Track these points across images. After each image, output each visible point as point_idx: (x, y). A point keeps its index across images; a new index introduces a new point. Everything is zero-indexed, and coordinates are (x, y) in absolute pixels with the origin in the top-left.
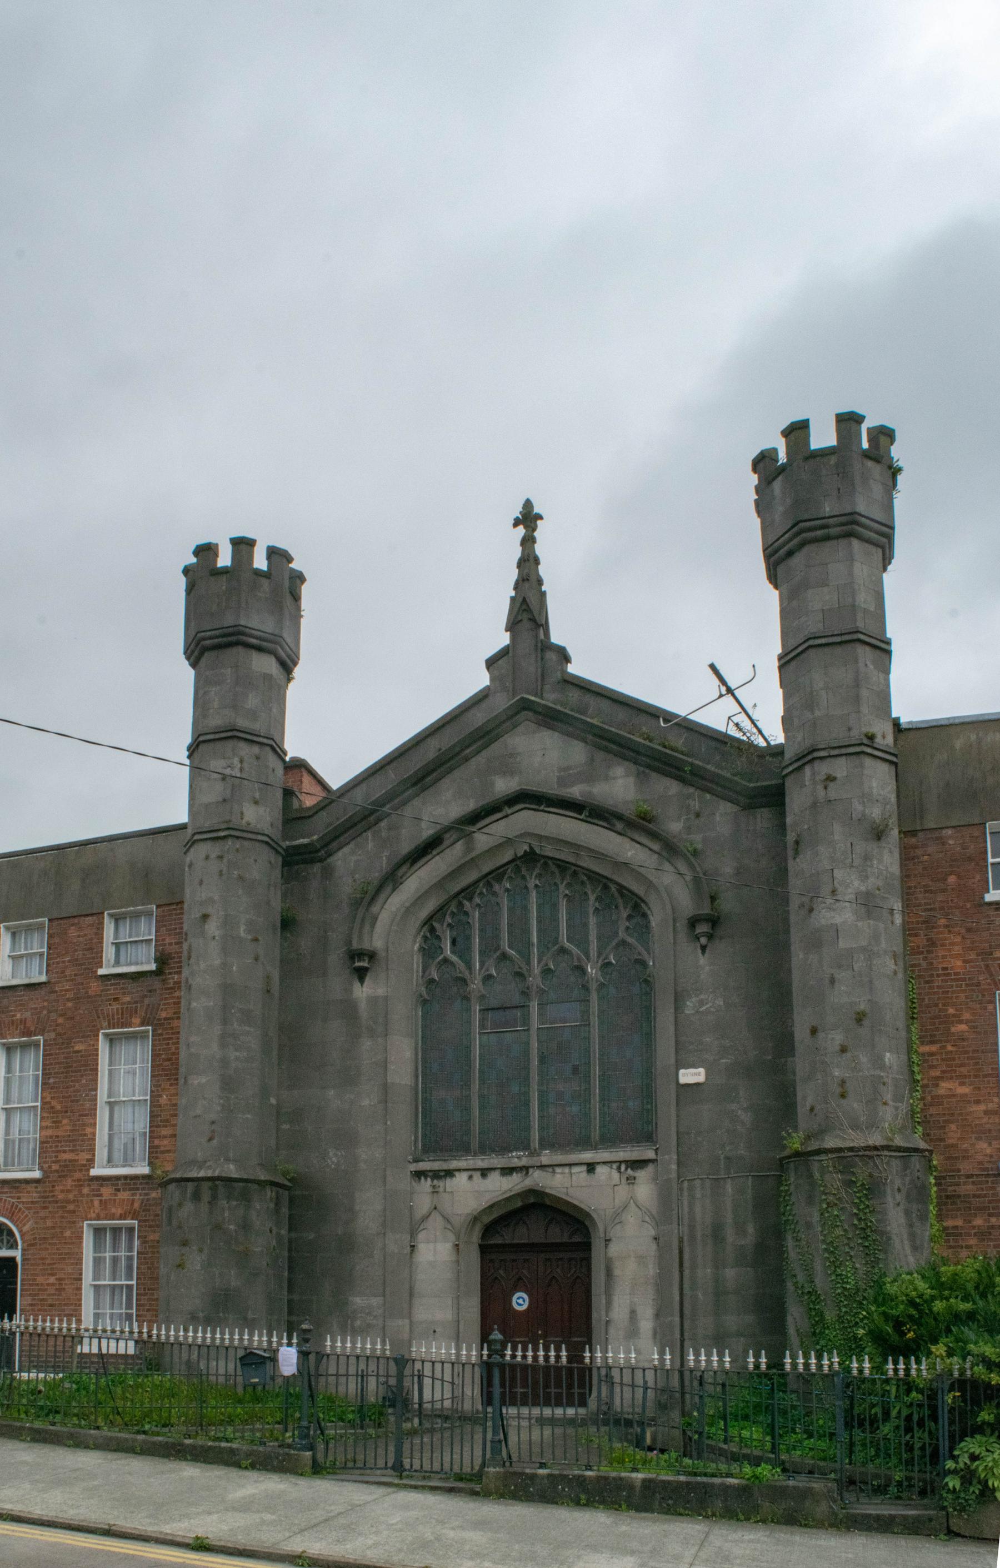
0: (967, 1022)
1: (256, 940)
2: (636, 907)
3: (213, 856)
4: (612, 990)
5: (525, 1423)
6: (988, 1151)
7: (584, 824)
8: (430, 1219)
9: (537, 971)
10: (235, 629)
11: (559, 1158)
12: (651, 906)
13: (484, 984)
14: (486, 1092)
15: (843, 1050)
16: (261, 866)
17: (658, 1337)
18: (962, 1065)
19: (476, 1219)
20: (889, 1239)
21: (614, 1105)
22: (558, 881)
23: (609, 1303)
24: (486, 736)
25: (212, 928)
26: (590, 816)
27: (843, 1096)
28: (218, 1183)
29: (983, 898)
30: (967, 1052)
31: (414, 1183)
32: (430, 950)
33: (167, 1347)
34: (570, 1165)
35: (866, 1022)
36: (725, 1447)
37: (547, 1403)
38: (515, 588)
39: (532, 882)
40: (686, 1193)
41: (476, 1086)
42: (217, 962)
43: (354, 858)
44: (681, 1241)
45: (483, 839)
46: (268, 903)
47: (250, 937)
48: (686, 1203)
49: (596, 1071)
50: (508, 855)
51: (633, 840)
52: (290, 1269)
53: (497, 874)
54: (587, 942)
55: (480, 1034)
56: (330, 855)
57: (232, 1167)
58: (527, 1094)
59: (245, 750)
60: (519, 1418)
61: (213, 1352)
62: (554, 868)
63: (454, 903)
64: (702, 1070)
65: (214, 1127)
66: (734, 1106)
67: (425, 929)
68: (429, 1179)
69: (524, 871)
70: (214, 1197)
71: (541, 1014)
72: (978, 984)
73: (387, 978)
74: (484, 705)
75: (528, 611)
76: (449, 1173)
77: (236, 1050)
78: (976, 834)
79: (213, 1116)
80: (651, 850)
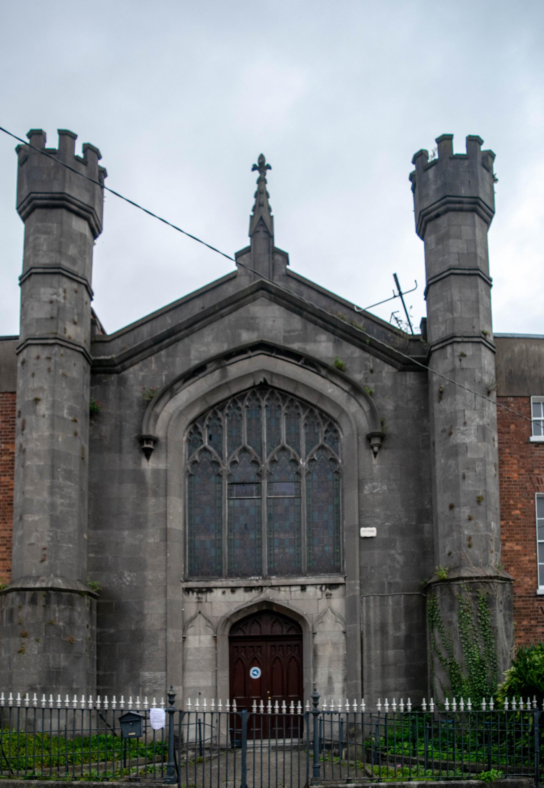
0: (520, 509)
1: (75, 421)
2: (331, 425)
3: (43, 356)
4: (315, 477)
5: (265, 750)
6: (531, 583)
7: (301, 369)
8: (197, 619)
9: (267, 461)
10: (62, 196)
11: (283, 581)
12: (341, 425)
13: (231, 466)
14: (232, 537)
15: (470, 519)
16: (77, 369)
17: (346, 693)
18: (518, 534)
19: (228, 620)
20: (497, 631)
21: (316, 549)
22: (281, 405)
23: (315, 673)
24: (237, 302)
25: (43, 408)
26: (305, 363)
27: (470, 546)
28: (51, 592)
29: (529, 439)
30: (519, 526)
31: (185, 597)
32: (193, 441)
33: (15, 711)
34: (290, 586)
35: (483, 503)
36: (415, 758)
37: (273, 737)
38: (254, 210)
39: (264, 403)
40: (364, 604)
41: (225, 533)
42: (47, 433)
43: (142, 374)
44: (362, 634)
45: (237, 368)
46: (83, 396)
47: (71, 418)
48: (364, 611)
49: (304, 526)
50: (249, 384)
51: (332, 382)
52: (98, 654)
53: (240, 396)
54: (299, 445)
55: (228, 499)
56: (124, 369)
57: (60, 581)
58: (260, 539)
59: (67, 284)
60: (262, 747)
61: (47, 712)
62: (278, 395)
63: (211, 411)
64: (374, 529)
65: (45, 552)
66: (393, 552)
67: (192, 426)
68: (195, 594)
69: (258, 395)
70: (48, 602)
71: (269, 489)
72: (526, 488)
73: (167, 457)
74: (233, 283)
75: (261, 223)
76: (209, 590)
77: (62, 498)
78: (526, 402)
79: (44, 544)
80: (343, 389)
